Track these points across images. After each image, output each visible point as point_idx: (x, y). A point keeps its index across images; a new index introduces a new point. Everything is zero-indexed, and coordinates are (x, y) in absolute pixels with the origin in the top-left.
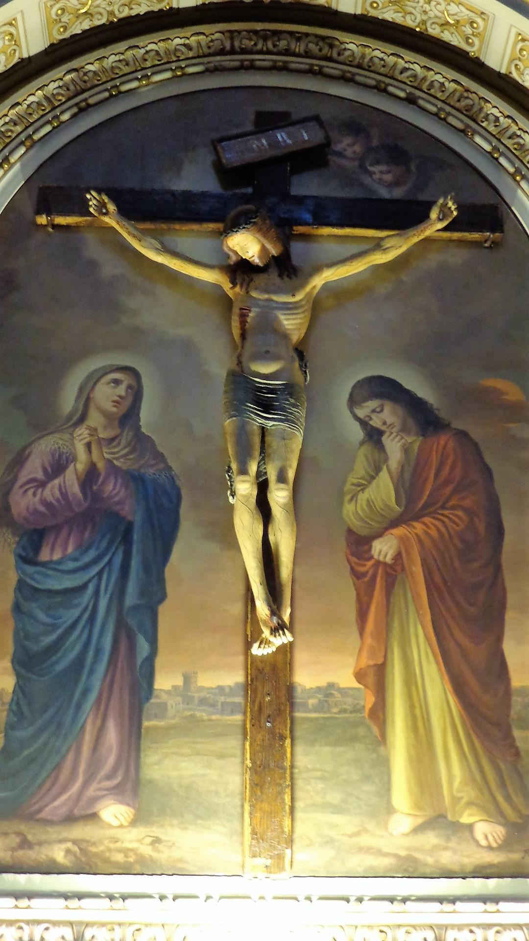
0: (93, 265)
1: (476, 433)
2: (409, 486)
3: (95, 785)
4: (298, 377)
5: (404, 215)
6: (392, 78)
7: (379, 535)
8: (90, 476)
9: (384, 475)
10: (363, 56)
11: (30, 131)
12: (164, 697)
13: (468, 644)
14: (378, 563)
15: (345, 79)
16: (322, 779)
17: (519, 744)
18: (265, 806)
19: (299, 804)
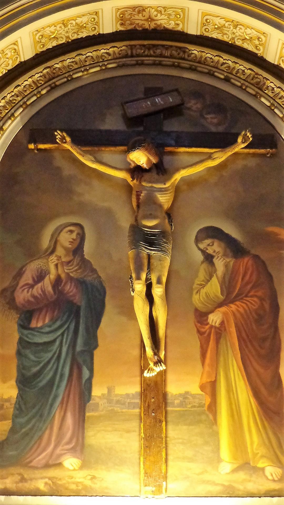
0: (59, 169)
1: (264, 256)
2: (228, 285)
3: (60, 448)
4: (168, 227)
5: (224, 141)
6: (217, 68)
7: (212, 312)
8: (58, 281)
9: (214, 279)
12: (97, 400)
13: (261, 370)
14: (212, 327)
15: (192, 69)
16: (182, 443)
19: (170, 457)
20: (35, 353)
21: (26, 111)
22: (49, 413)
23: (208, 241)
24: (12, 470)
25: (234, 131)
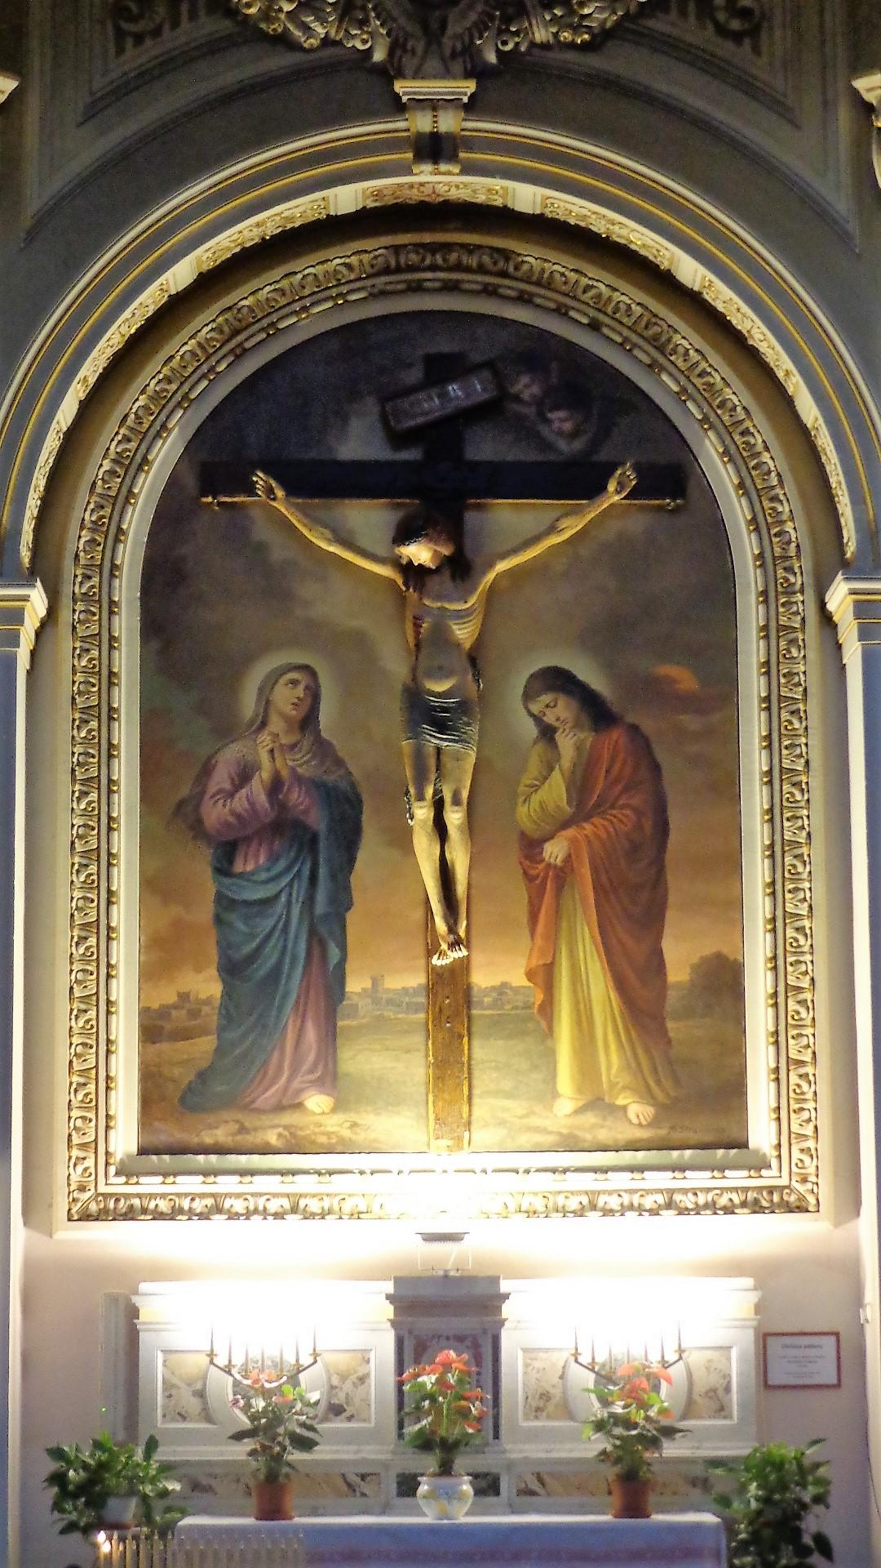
0: (261, 548)
1: (648, 725)
2: (580, 787)
3: (299, 1079)
4: (472, 690)
5: (577, 481)
6: (574, 298)
7: (550, 837)
8: (275, 787)
9: (556, 775)
10: (543, 270)
11: (186, 388)
12: (355, 999)
13: (630, 943)
14: (549, 865)
15: (524, 299)
16: (497, 1069)
17: (671, 1034)
18: (446, 1096)
20: (247, 919)
21: (189, 411)
22: (278, 1017)
23: (546, 698)
24: (226, 1115)
25: (603, 456)
